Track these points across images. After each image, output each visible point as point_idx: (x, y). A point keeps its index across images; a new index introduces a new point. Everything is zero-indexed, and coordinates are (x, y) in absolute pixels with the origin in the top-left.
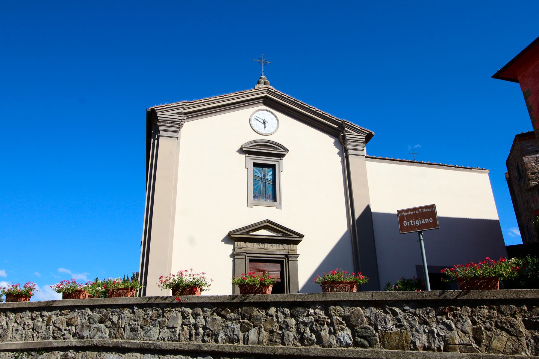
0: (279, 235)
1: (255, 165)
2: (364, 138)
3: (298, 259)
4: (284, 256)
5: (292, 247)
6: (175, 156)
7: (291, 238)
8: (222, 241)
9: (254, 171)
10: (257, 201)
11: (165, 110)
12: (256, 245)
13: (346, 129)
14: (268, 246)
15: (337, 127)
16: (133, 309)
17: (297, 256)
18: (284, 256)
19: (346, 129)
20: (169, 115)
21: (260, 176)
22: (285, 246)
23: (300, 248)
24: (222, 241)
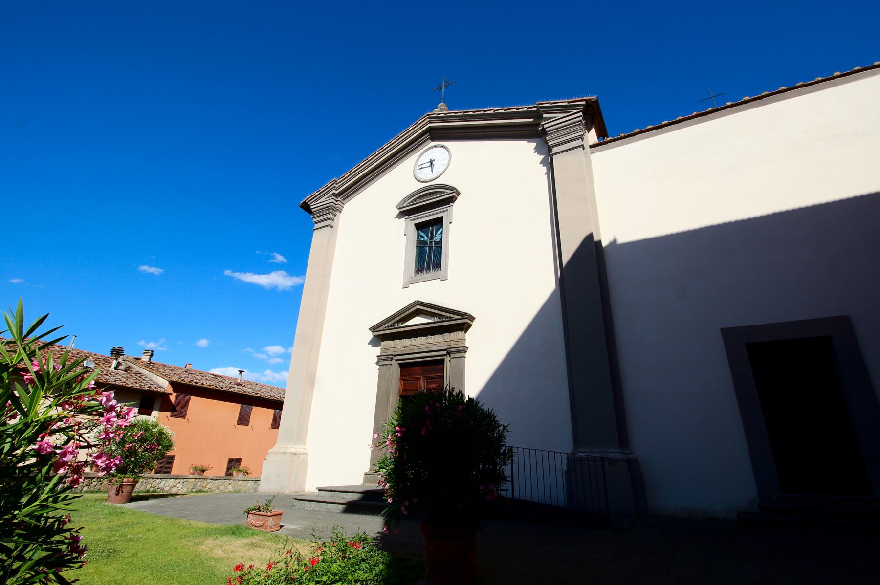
0: (436, 319)
1: (419, 227)
2: (581, 114)
3: (467, 355)
4: (445, 353)
5: (457, 335)
6: (330, 246)
7: (460, 322)
8: (369, 343)
9: (418, 235)
10: (420, 276)
11: (316, 198)
12: (406, 342)
13: (545, 115)
14: (422, 340)
15: (531, 120)
16: (17, 458)
17: (463, 350)
18: (445, 353)
19: (545, 115)
20: (324, 201)
21: (426, 239)
22: (446, 335)
23: (470, 338)
24: (369, 343)
